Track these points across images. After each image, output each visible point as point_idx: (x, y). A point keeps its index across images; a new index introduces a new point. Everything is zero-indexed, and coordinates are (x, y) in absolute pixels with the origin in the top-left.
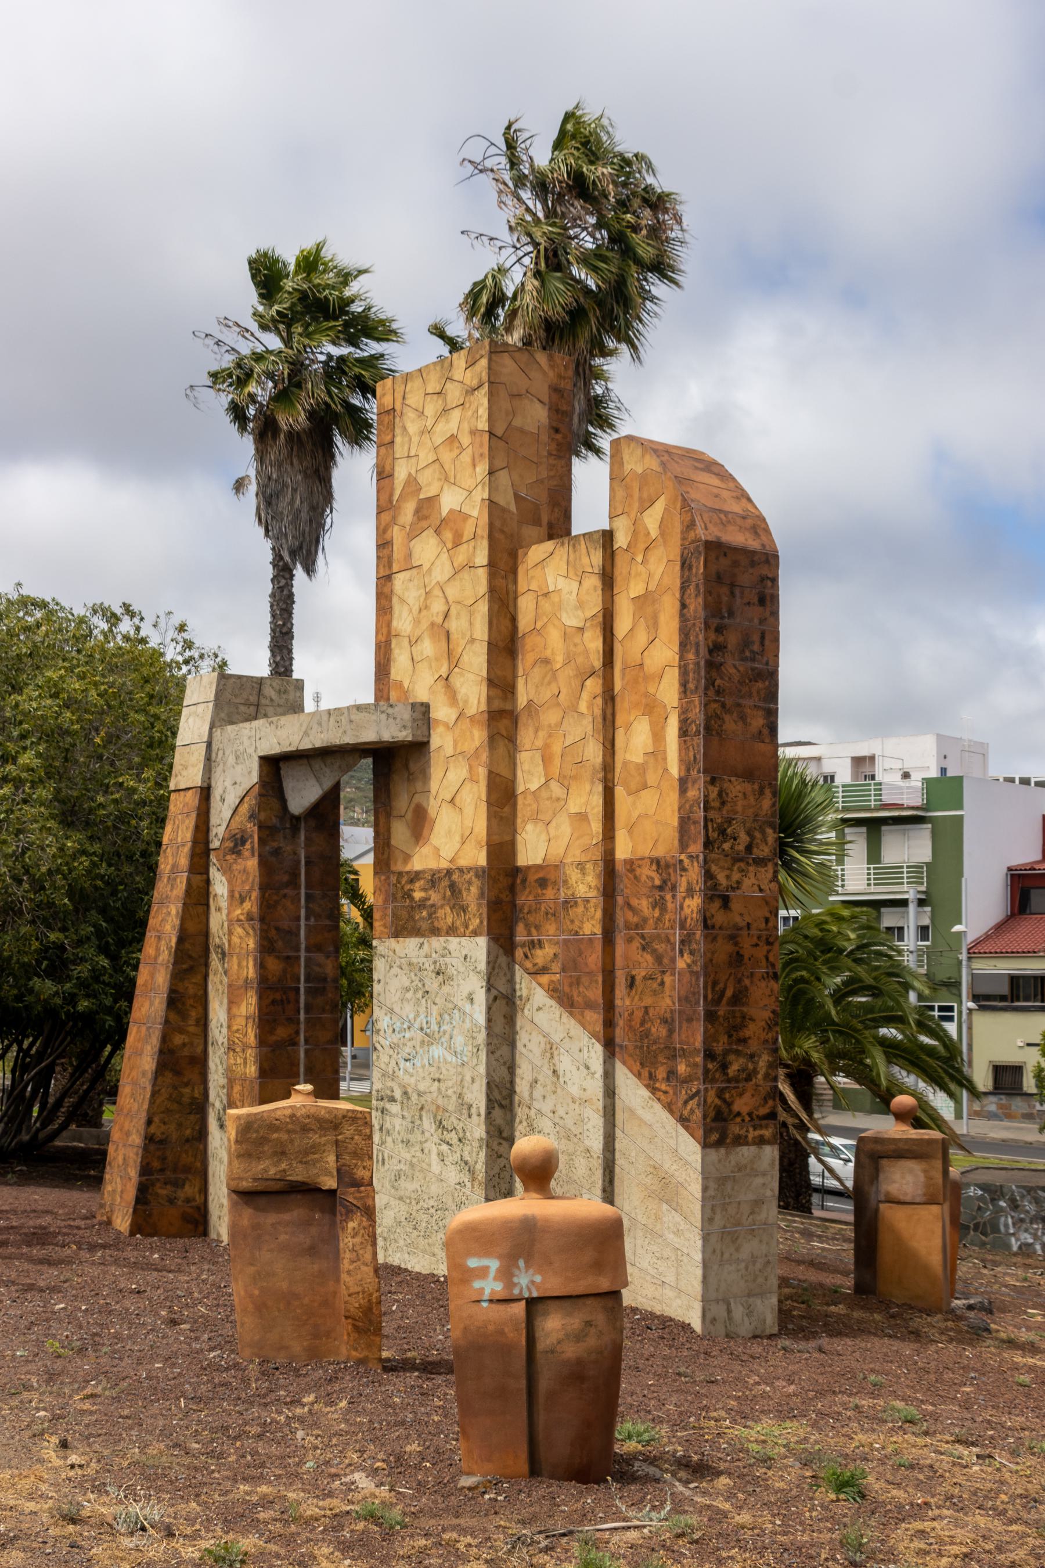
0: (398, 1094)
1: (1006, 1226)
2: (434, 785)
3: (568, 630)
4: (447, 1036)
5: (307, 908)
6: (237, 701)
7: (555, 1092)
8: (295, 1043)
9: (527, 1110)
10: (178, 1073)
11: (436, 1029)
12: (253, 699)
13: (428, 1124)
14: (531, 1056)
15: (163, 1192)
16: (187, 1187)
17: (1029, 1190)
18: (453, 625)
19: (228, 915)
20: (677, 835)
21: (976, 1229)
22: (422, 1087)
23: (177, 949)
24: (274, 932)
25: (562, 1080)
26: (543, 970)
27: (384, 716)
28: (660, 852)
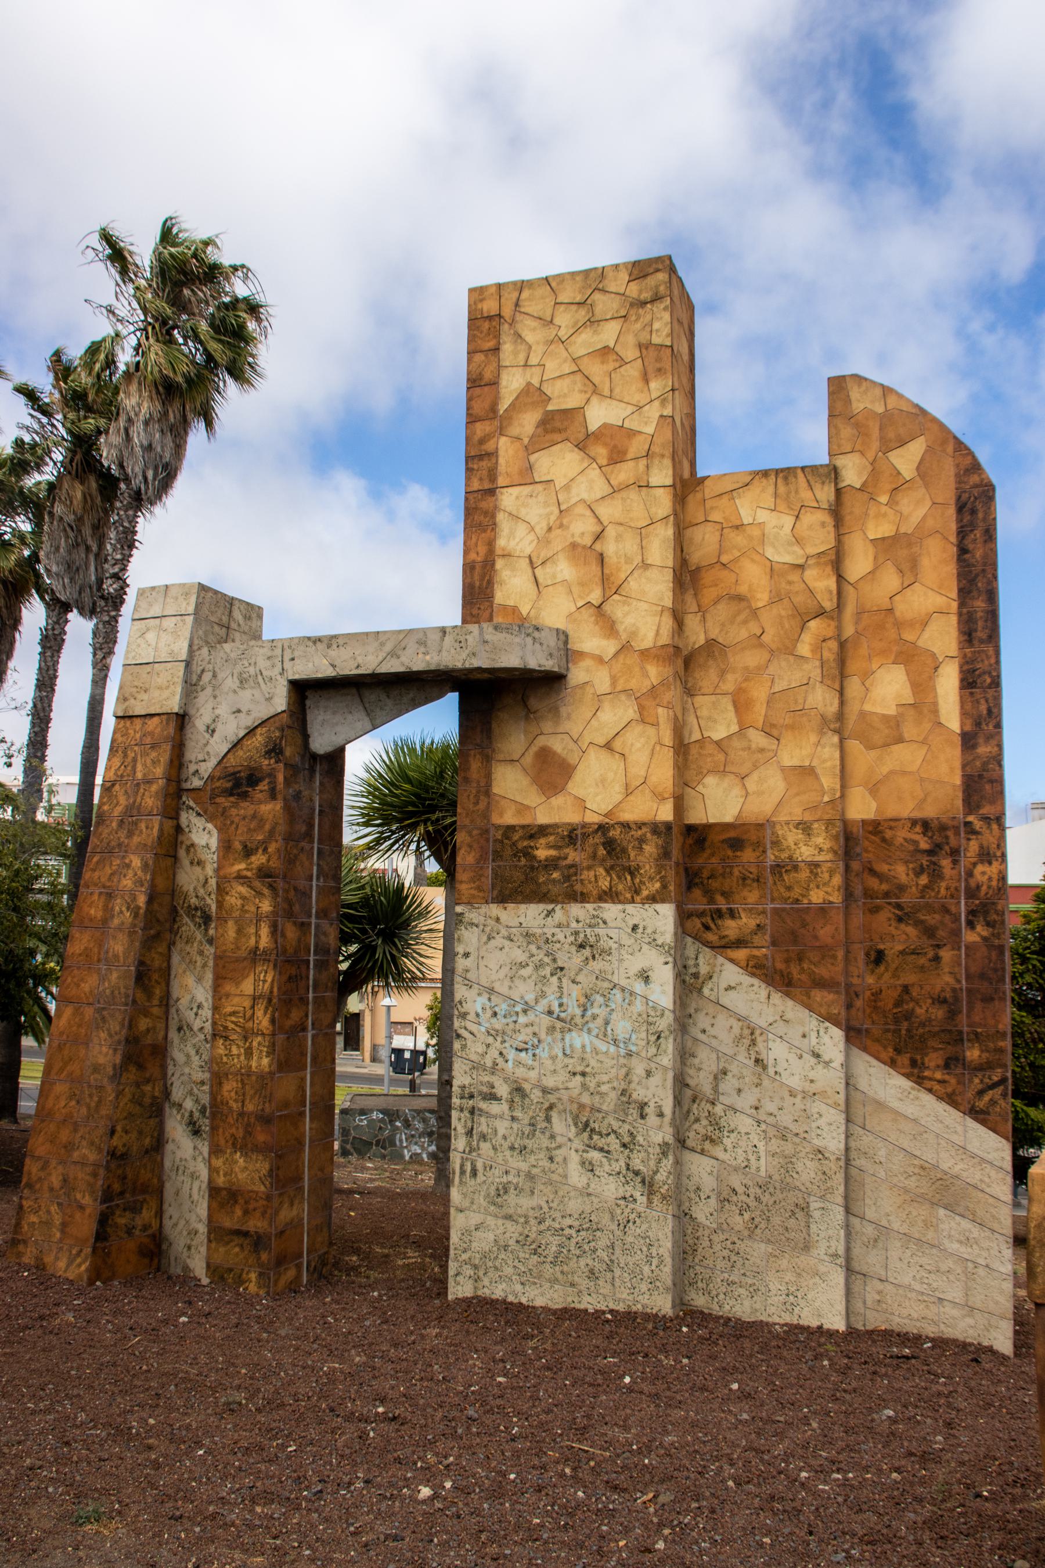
0: (503, 1090)
1: (401, 1141)
3: (776, 567)
4: (600, 1021)
5: (318, 865)
6: (213, 619)
8: (304, 1029)
9: (709, 1106)
10: (141, 1067)
11: (578, 1012)
12: (225, 619)
13: (560, 1125)
14: (714, 1043)
15: (121, 1221)
16: (144, 1211)
17: (419, 1112)
18: (610, 548)
19: (217, 871)
20: (960, 795)
21: (377, 1145)
22: (550, 1082)
23: (148, 911)
24: (292, 893)
25: (771, 1071)
26: (739, 943)
27: (529, 640)
28: (930, 812)
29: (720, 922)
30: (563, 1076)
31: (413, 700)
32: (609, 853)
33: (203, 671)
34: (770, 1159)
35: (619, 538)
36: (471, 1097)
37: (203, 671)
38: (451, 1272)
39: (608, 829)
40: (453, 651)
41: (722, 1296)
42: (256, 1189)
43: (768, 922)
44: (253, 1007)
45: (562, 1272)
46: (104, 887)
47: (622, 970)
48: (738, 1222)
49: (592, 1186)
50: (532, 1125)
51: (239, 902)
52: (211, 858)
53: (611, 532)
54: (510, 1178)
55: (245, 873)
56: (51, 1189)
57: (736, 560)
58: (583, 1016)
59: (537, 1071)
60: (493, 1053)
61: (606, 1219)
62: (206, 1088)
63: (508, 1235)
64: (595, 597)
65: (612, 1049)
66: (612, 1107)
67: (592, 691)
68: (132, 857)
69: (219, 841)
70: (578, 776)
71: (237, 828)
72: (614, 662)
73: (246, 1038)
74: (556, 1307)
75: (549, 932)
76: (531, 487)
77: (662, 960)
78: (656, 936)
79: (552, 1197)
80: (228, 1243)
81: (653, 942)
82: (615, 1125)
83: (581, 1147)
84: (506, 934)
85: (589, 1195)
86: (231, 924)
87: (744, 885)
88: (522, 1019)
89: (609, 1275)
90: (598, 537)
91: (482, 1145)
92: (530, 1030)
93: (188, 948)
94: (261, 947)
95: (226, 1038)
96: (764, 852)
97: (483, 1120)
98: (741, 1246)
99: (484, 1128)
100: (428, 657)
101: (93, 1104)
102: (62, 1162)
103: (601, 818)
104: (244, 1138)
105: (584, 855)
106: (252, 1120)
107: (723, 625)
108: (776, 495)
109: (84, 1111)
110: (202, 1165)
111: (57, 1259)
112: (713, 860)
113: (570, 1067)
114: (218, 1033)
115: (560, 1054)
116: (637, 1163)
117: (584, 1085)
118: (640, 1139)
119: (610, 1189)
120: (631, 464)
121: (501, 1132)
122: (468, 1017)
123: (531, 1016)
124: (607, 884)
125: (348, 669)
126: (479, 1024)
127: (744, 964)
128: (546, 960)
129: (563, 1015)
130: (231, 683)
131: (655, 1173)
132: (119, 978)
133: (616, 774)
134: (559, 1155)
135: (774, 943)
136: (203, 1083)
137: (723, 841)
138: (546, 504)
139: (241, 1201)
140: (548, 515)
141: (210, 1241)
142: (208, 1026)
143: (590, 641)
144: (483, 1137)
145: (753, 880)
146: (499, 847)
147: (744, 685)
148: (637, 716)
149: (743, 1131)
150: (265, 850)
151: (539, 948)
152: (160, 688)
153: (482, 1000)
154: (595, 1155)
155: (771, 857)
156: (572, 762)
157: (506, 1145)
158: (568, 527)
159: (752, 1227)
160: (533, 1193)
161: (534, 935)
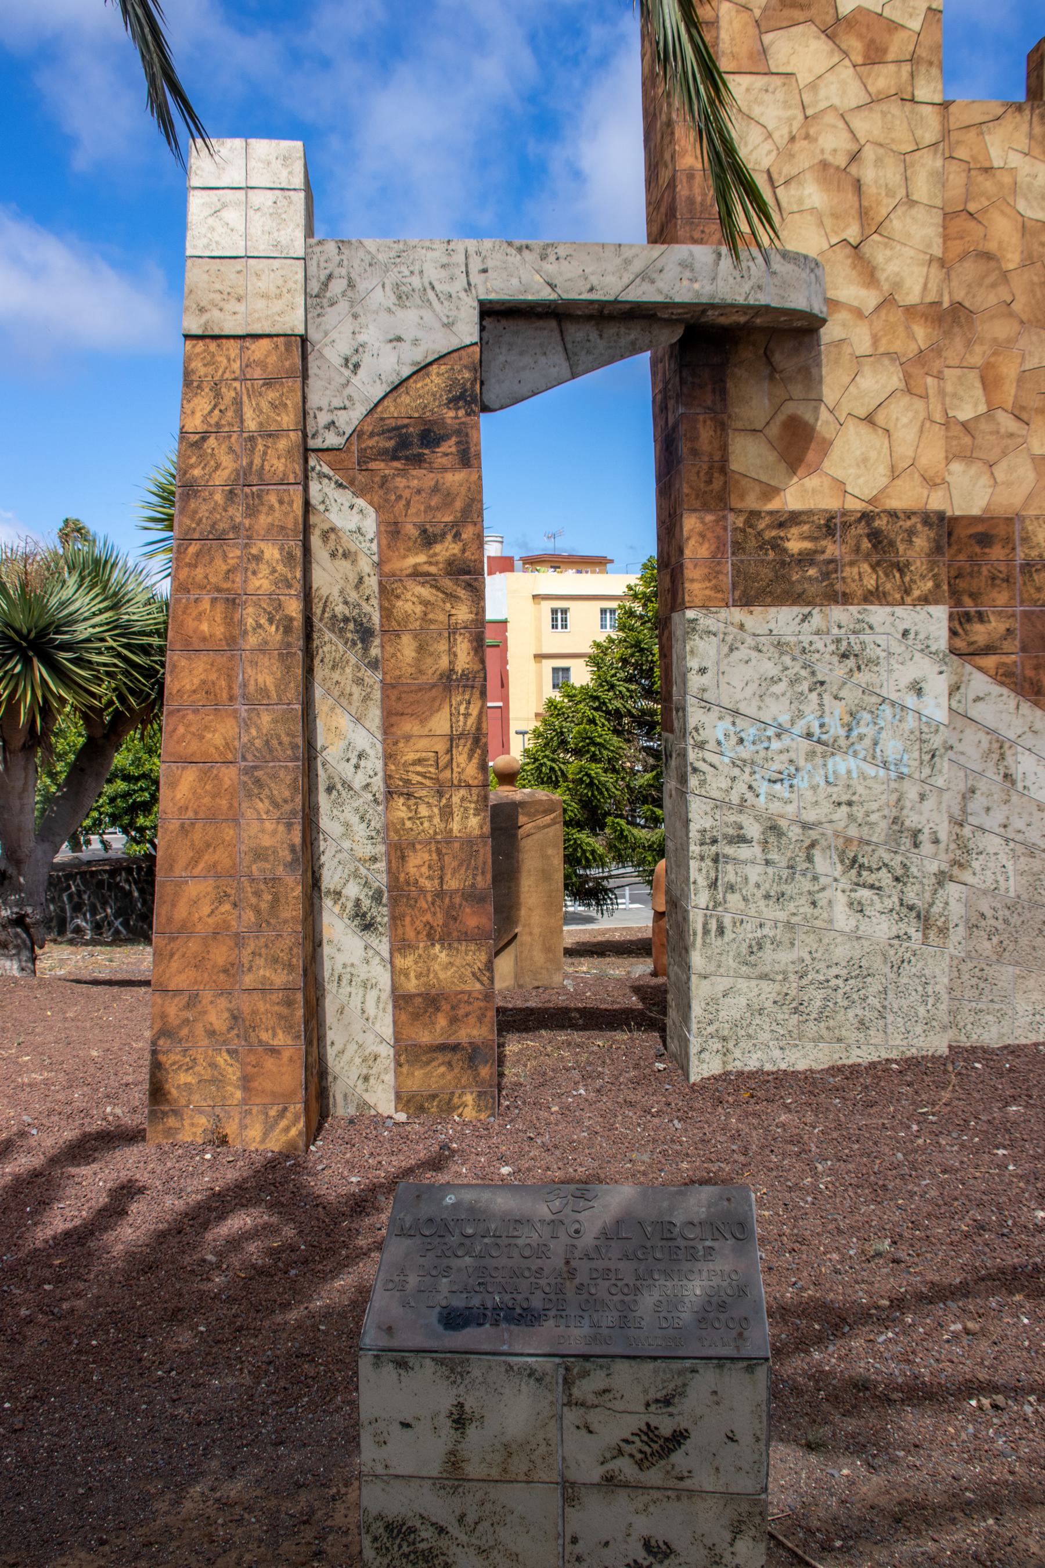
0: (753, 830)
2: (830, 394)
3: (1028, 224)
4: (867, 742)
7: (1006, 802)
11: (842, 732)
13: (825, 864)
18: (869, 174)
19: (379, 565)
22: (810, 816)
25: (1020, 786)
26: (988, 650)
29: (968, 627)
30: (826, 807)
31: (633, 343)
32: (874, 546)
33: (330, 277)
34: (1019, 878)
35: (878, 162)
36: (714, 841)
37: (330, 277)
38: (694, 1049)
39: (873, 519)
40: (731, 280)
41: (970, 1026)
42: (467, 988)
43: (1017, 625)
44: (450, 751)
45: (828, 1028)
46: (219, 590)
47: (892, 683)
48: (987, 947)
49: (862, 928)
50: (791, 867)
51: (419, 609)
52: (368, 552)
53: (869, 153)
54: (766, 931)
55: (426, 568)
56: (212, 1033)
57: (984, 210)
58: (848, 737)
59: (794, 805)
60: (741, 787)
61: (878, 963)
62: (382, 865)
63: (763, 996)
64: (852, 233)
65: (882, 772)
66: (882, 838)
67: (849, 351)
68: (262, 545)
69: (379, 524)
70: (835, 452)
71: (408, 504)
72: (874, 317)
73: (440, 794)
74: (822, 1067)
75: (805, 639)
76: (766, 78)
77: (936, 668)
78: (930, 643)
79: (815, 946)
80: (428, 1063)
81: (926, 650)
82: (887, 857)
83: (848, 887)
84: (753, 644)
85: (859, 938)
86: (406, 639)
87: (993, 585)
88: (775, 745)
89: (881, 1022)
90: (855, 157)
91: (730, 897)
92: (785, 757)
93: (336, 676)
94: (459, 669)
95: (409, 795)
96: (1014, 549)
97: (730, 868)
98: (989, 972)
99: (731, 877)
100: (696, 286)
101: (264, 906)
102: (225, 992)
103: (864, 504)
104: (445, 925)
105: (845, 549)
106: (457, 900)
107: (969, 286)
108: (1031, 136)
109: (250, 916)
110: (380, 968)
111: (243, 1127)
112: (961, 557)
113: (834, 797)
114: (395, 790)
115: (822, 783)
116: (911, 897)
117: (850, 816)
118: (914, 870)
119: (882, 928)
120: (892, 68)
121: (753, 879)
122: (707, 746)
123: (786, 740)
124: (873, 582)
125: (574, 290)
126: (722, 754)
127: (992, 672)
128: (804, 673)
129: (824, 737)
130: (382, 298)
131: (931, 905)
132: (275, 721)
133: (879, 453)
134: (822, 898)
135: (1024, 649)
136: (374, 859)
137: (970, 536)
138: (786, 105)
139: (445, 1006)
140: (790, 120)
141: (399, 1064)
142: (378, 783)
143: (847, 289)
144: (731, 888)
145: (1003, 580)
146: (740, 537)
147: (992, 359)
148: (902, 385)
149: (992, 852)
150: (457, 536)
151: (794, 659)
152: (265, 296)
153: (726, 724)
154: (864, 894)
155: (1020, 555)
156: (827, 436)
157: (759, 894)
158: (816, 140)
159: (1001, 949)
160: (792, 944)
161: (787, 644)
